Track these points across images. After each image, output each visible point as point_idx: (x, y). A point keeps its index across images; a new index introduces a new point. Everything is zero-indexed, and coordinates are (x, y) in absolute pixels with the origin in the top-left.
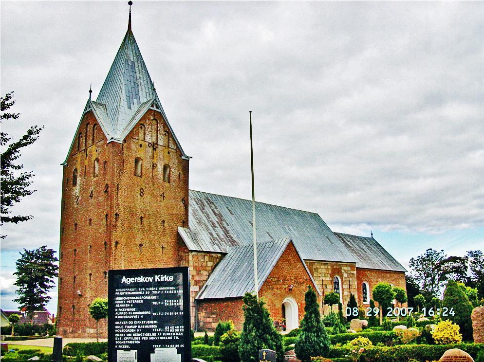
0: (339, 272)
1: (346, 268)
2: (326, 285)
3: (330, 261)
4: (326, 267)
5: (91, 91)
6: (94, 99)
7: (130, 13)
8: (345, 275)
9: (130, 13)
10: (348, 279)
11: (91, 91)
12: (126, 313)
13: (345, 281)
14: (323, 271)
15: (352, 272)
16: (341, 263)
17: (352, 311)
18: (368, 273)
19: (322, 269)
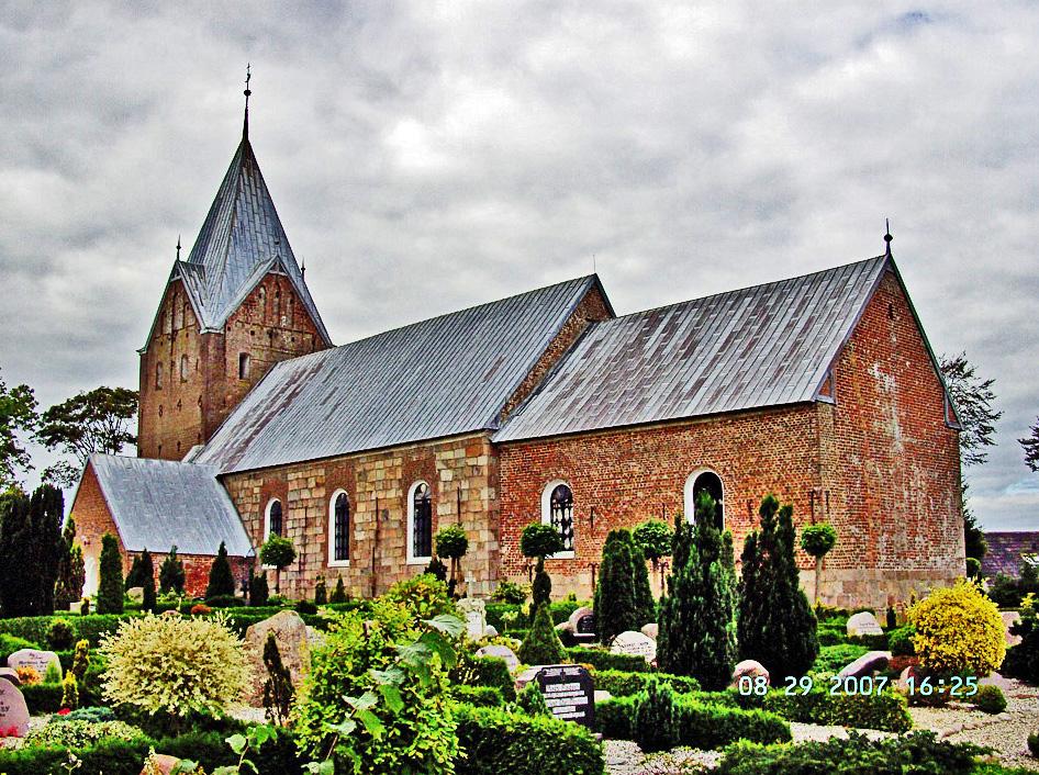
0: (428, 471)
1: (449, 455)
2: (386, 512)
3: (343, 455)
4: (389, 463)
5: (179, 247)
6: (184, 257)
7: (246, 110)
8: (447, 475)
9: (246, 110)
10: (456, 485)
11: (179, 247)
12: (247, 188)
13: (445, 493)
14: (380, 475)
15: (471, 462)
16: (335, 460)
17: (754, 685)
18: (572, 451)
19: (378, 470)
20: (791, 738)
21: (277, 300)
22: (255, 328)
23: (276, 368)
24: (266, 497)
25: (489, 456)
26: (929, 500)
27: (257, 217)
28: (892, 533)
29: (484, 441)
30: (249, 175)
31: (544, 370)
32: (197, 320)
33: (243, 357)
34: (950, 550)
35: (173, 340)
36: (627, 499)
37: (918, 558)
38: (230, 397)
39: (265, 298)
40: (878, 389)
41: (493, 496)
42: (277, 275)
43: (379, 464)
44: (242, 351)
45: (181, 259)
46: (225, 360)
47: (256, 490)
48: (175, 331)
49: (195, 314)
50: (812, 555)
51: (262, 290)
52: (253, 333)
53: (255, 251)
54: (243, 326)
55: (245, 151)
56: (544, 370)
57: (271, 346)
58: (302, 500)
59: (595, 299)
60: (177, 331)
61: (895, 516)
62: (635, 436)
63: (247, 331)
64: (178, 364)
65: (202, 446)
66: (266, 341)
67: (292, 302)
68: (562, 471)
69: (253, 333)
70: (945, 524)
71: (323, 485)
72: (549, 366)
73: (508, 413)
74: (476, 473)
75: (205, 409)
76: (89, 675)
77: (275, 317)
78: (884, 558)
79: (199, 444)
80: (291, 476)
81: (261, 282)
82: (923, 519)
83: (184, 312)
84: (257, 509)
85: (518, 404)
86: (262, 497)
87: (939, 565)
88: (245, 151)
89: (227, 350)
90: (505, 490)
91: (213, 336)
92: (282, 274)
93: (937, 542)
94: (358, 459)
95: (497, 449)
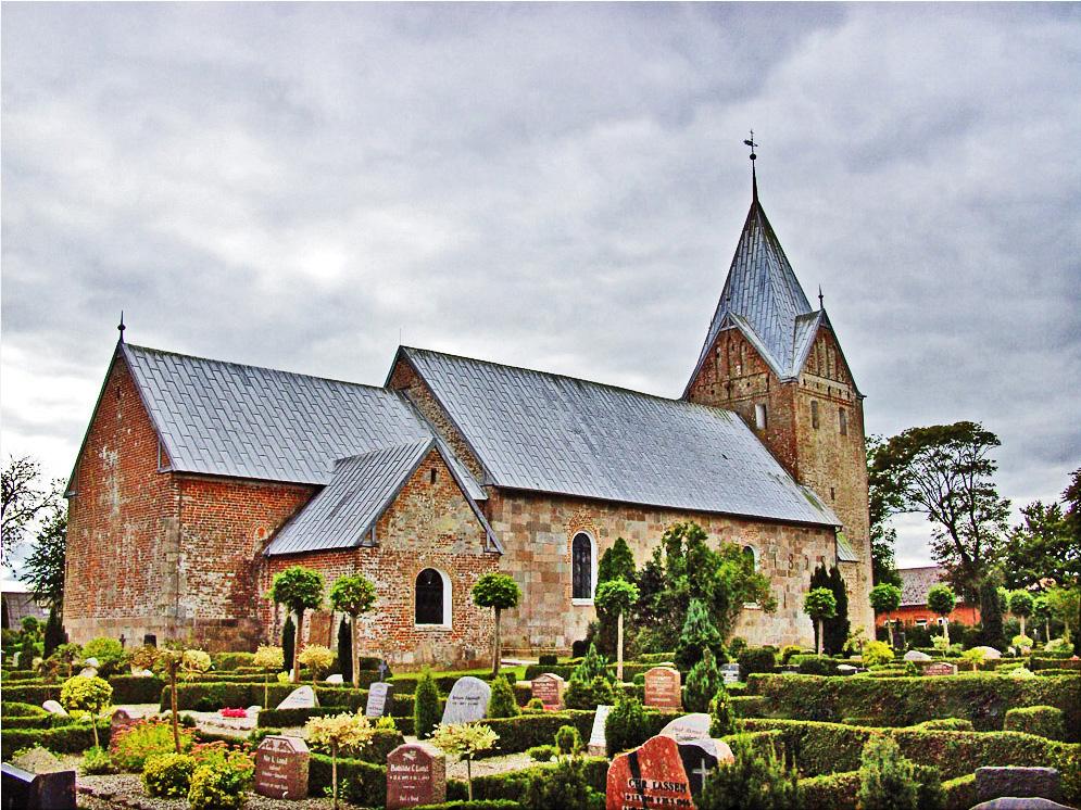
11: (821, 297)
20: (73, 773)
26: (137, 552)
28: (106, 587)
34: (153, 598)
37: (124, 608)
40: (105, 467)
50: (930, 600)
57: (729, 398)
61: (109, 573)
69: (713, 392)
70: (150, 572)
78: (99, 608)
82: (130, 571)
87: (141, 613)
93: (141, 590)
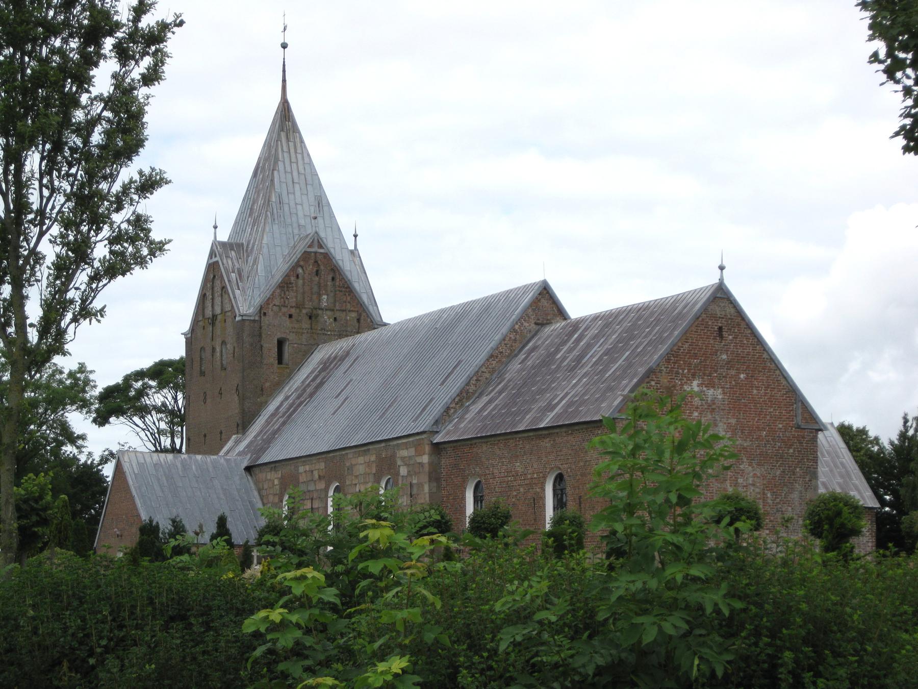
4: (367, 458)
8: (403, 471)
9: (284, 65)
12: (286, 155)
21: (317, 279)
22: (293, 311)
23: (316, 351)
24: (284, 487)
25: (430, 455)
27: (297, 187)
29: (426, 442)
30: (288, 140)
31: (487, 375)
32: (232, 306)
33: (281, 343)
35: (213, 324)
36: (515, 493)
38: (267, 384)
39: (304, 279)
41: (434, 490)
42: (315, 253)
43: (361, 460)
44: (279, 335)
45: (218, 239)
46: (262, 346)
47: (276, 482)
48: (214, 317)
49: (230, 300)
51: (300, 270)
52: (290, 316)
53: (295, 225)
54: (280, 310)
55: (285, 114)
56: (487, 375)
57: (311, 329)
58: (309, 491)
59: (545, 303)
60: (216, 316)
62: (519, 441)
63: (284, 314)
64: (218, 350)
65: (240, 436)
66: (306, 324)
67: (333, 279)
68: (478, 469)
71: (324, 477)
72: (492, 372)
73: (449, 416)
74: (421, 470)
75: (242, 399)
76: (35, 531)
77: (315, 297)
79: (237, 433)
80: (301, 469)
81: (298, 261)
83: (222, 296)
84: (276, 500)
85: (460, 407)
86: (281, 488)
88: (285, 114)
89: (264, 336)
90: (444, 483)
91: (247, 323)
92: (322, 251)
94: (347, 454)
95: (438, 448)
